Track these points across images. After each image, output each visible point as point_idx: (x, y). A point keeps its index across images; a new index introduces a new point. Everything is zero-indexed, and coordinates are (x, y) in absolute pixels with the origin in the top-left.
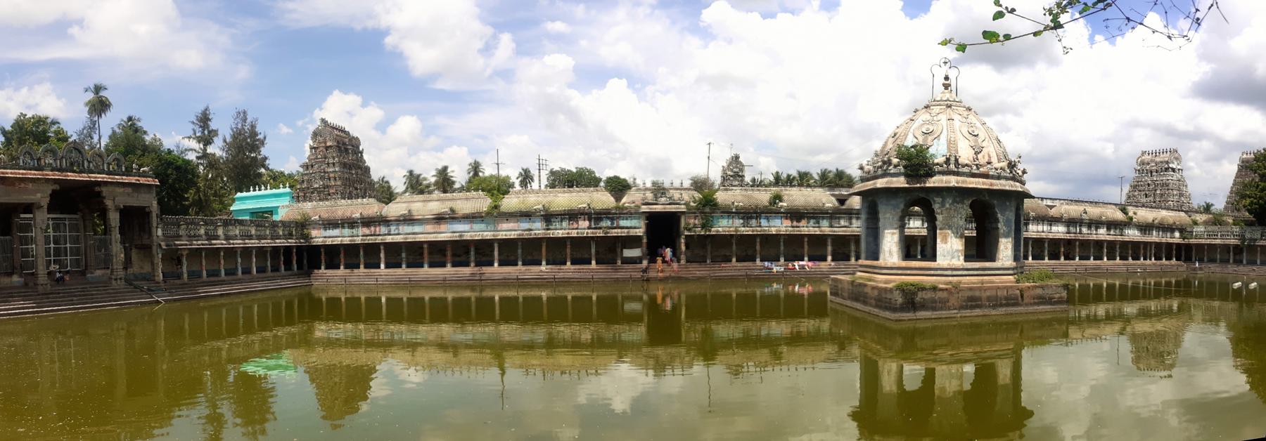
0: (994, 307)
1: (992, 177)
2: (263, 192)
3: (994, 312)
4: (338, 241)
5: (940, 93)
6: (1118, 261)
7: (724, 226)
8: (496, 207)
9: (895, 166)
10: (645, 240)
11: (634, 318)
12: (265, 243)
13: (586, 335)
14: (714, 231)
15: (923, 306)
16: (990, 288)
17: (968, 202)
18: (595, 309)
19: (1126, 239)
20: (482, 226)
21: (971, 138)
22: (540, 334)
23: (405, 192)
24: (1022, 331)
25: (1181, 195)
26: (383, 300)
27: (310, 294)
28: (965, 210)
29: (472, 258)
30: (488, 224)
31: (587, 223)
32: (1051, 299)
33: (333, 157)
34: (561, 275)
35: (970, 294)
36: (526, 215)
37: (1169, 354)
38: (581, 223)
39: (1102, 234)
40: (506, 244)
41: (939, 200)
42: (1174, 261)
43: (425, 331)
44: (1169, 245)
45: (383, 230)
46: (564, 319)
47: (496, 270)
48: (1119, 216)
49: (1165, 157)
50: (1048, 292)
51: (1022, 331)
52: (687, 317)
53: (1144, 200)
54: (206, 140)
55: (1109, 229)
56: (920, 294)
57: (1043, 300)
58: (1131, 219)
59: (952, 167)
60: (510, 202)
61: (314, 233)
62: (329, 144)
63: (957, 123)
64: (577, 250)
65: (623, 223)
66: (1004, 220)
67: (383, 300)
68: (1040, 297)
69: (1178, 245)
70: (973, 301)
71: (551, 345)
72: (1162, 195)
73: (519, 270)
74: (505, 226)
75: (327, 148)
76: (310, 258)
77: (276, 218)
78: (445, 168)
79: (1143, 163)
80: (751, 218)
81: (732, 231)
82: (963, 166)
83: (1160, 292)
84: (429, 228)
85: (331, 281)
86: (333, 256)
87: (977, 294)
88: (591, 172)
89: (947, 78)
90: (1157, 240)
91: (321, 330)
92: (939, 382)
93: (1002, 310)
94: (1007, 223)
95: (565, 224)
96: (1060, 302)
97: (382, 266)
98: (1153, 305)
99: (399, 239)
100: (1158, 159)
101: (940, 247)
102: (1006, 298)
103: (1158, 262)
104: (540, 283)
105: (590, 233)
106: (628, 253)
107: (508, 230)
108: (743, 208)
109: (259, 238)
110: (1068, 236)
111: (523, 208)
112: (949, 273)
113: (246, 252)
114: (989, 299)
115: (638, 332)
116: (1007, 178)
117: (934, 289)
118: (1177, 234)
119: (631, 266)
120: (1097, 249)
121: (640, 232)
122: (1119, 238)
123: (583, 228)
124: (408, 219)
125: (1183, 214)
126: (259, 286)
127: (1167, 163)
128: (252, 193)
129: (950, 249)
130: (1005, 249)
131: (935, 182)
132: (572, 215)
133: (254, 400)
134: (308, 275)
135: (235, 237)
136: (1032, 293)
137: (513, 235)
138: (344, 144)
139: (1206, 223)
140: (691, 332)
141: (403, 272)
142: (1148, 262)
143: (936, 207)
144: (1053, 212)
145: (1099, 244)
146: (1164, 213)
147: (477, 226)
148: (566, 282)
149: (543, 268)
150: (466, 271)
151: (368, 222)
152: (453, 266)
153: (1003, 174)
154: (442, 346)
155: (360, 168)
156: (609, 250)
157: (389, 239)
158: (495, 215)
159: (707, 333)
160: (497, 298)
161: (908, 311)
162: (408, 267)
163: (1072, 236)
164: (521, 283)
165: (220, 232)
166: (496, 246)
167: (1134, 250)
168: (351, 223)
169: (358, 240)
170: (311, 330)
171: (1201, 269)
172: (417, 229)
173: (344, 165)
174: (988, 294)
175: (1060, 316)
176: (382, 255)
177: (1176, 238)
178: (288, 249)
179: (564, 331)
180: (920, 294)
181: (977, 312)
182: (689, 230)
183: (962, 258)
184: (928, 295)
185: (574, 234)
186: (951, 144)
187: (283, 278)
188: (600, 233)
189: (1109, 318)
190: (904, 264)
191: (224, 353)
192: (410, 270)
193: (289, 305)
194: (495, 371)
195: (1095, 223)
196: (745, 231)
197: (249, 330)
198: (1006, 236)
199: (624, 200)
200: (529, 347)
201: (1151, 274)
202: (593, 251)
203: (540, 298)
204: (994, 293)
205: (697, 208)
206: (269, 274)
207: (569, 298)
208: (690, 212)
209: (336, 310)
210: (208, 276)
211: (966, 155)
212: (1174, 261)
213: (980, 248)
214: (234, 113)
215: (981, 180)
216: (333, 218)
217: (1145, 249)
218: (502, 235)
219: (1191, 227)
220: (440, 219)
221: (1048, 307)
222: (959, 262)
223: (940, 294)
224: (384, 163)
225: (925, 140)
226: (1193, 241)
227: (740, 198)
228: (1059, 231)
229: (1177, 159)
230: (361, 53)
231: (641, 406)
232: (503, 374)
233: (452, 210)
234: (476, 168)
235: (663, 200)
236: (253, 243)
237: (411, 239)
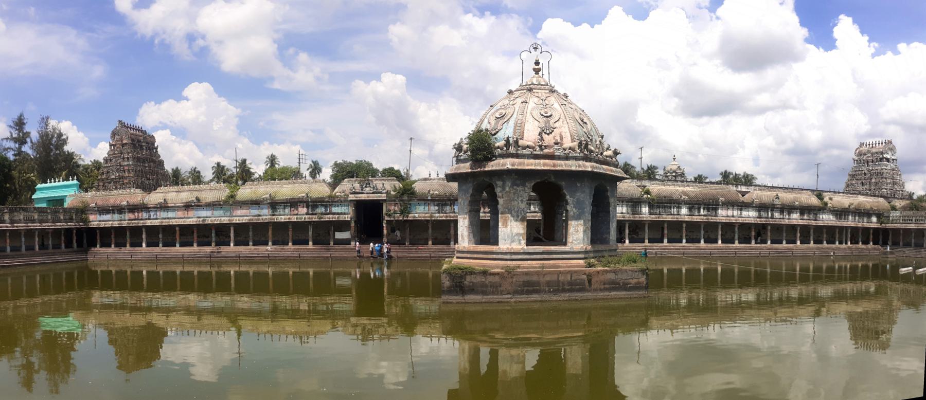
0: (556, 292)
1: (559, 158)
2: (57, 184)
3: (555, 298)
4: (109, 224)
5: (530, 77)
6: (812, 244)
7: (420, 212)
8: (232, 196)
9: (465, 152)
10: (353, 225)
11: (343, 292)
12: (45, 225)
13: (304, 305)
14: (411, 217)
15: (472, 290)
16: (550, 273)
17: (530, 185)
18: (311, 283)
19: (820, 223)
20: (221, 212)
21: (542, 120)
22: (266, 303)
23: (212, 181)
24: (589, 318)
25: (895, 183)
26: (144, 273)
27: (87, 266)
28: (527, 191)
29: (214, 239)
30: (226, 211)
31: (305, 210)
32: (625, 284)
33: (128, 153)
34: (281, 254)
35: (526, 278)
36: (256, 203)
37: (883, 332)
38: (300, 209)
39: (795, 218)
40: (241, 229)
41: (500, 183)
42: (871, 245)
43: (220, 300)
44: (866, 230)
45: (145, 215)
46: (285, 292)
47: (232, 249)
48: (814, 201)
49: (880, 148)
50: (622, 277)
51: (589, 318)
52: (389, 293)
53: (860, 188)
54: (21, 140)
55: (802, 214)
56: (468, 278)
57: (615, 286)
58: (826, 204)
59: (512, 150)
60: (245, 192)
61: (92, 217)
62: (124, 142)
63: (531, 105)
64: (296, 232)
65: (335, 210)
66: (577, 202)
67: (144, 273)
68: (613, 282)
69: (875, 230)
70: (529, 285)
71: (275, 313)
72: (876, 183)
73: (249, 250)
74: (239, 212)
75: (123, 145)
76: (88, 238)
77: (66, 205)
78: (244, 161)
79: (860, 154)
80: (446, 205)
81: (427, 217)
82: (524, 148)
83: (857, 274)
84: (180, 214)
85: (104, 257)
86: (108, 236)
87: (535, 278)
88: (370, 165)
89: (537, 63)
90: (853, 225)
91: (97, 297)
92: (503, 366)
93: (566, 296)
94: (579, 205)
95: (287, 211)
96: (637, 287)
97: (144, 245)
98: (848, 287)
99: (156, 223)
100: (874, 150)
101: (503, 231)
102: (570, 283)
103: (854, 246)
104: (269, 260)
105: (306, 218)
106: (339, 235)
107: (242, 216)
108: (438, 196)
109: (41, 222)
110: (759, 221)
111: (254, 197)
112: (508, 257)
113: (30, 233)
114: (549, 284)
115: (347, 304)
116: (576, 159)
117: (485, 273)
118: (874, 219)
119: (341, 246)
120: (676, 230)
121: (347, 218)
122: (813, 223)
123: (302, 214)
124: (164, 207)
125: (881, 200)
126: (37, 260)
127: (882, 153)
128: (48, 185)
129: (511, 233)
130: (577, 234)
131: (494, 165)
132: (293, 203)
133: (58, 352)
134: (86, 252)
135: (19, 221)
136: (602, 278)
137: (245, 220)
138: (139, 141)
139: (904, 208)
140: (393, 307)
141: (159, 249)
142: (844, 246)
143: (498, 190)
144: (747, 198)
145: (792, 228)
146: (861, 199)
147: (217, 213)
148: (286, 260)
149: (269, 248)
150: (208, 249)
151: (133, 208)
152: (198, 245)
153: (573, 154)
154: (189, 311)
155: (154, 162)
156: (323, 232)
157: (149, 223)
158: (231, 203)
159: (407, 308)
160: (232, 273)
161: (457, 294)
162: (164, 246)
163: (763, 221)
164: (250, 260)
165: (7, 217)
166: (232, 229)
167: (831, 234)
168: (120, 210)
169: (125, 224)
170: (89, 296)
171: (891, 253)
172: (171, 214)
173: (138, 160)
174: (548, 278)
175: (650, 298)
176: (144, 236)
177: (874, 222)
178: (68, 231)
179: (285, 301)
180: (468, 278)
181: (535, 297)
182: (389, 216)
183: (523, 242)
184: (479, 279)
185: (294, 219)
186: (520, 127)
187: (62, 254)
188: (315, 218)
189: (802, 301)
190: (532, 249)
191: (10, 313)
192: (165, 248)
193: (70, 276)
194: (233, 333)
195: (788, 208)
196: (439, 216)
197: (31, 294)
198: (577, 218)
199: (336, 190)
200: (257, 314)
201: (844, 258)
202: (310, 233)
203: (248, 273)
204: (555, 278)
205: (396, 196)
206: (51, 250)
207: (291, 273)
208: (390, 199)
209: (108, 281)
210: (11, 251)
211: (530, 136)
212: (871, 245)
213: (546, 231)
214: (39, 118)
215: (542, 161)
216: (109, 205)
217: (841, 233)
218: (236, 220)
219: (889, 211)
220: (188, 206)
221: (623, 293)
222: (521, 245)
223: (490, 279)
224: (175, 154)
225: (497, 123)
226: (889, 226)
227: (436, 187)
228: (750, 216)
229: (891, 150)
230: (168, 65)
231: (235, 375)
232: (239, 335)
233: (198, 199)
234: (272, 160)
235: (368, 189)
236: (37, 226)
237: (165, 223)
